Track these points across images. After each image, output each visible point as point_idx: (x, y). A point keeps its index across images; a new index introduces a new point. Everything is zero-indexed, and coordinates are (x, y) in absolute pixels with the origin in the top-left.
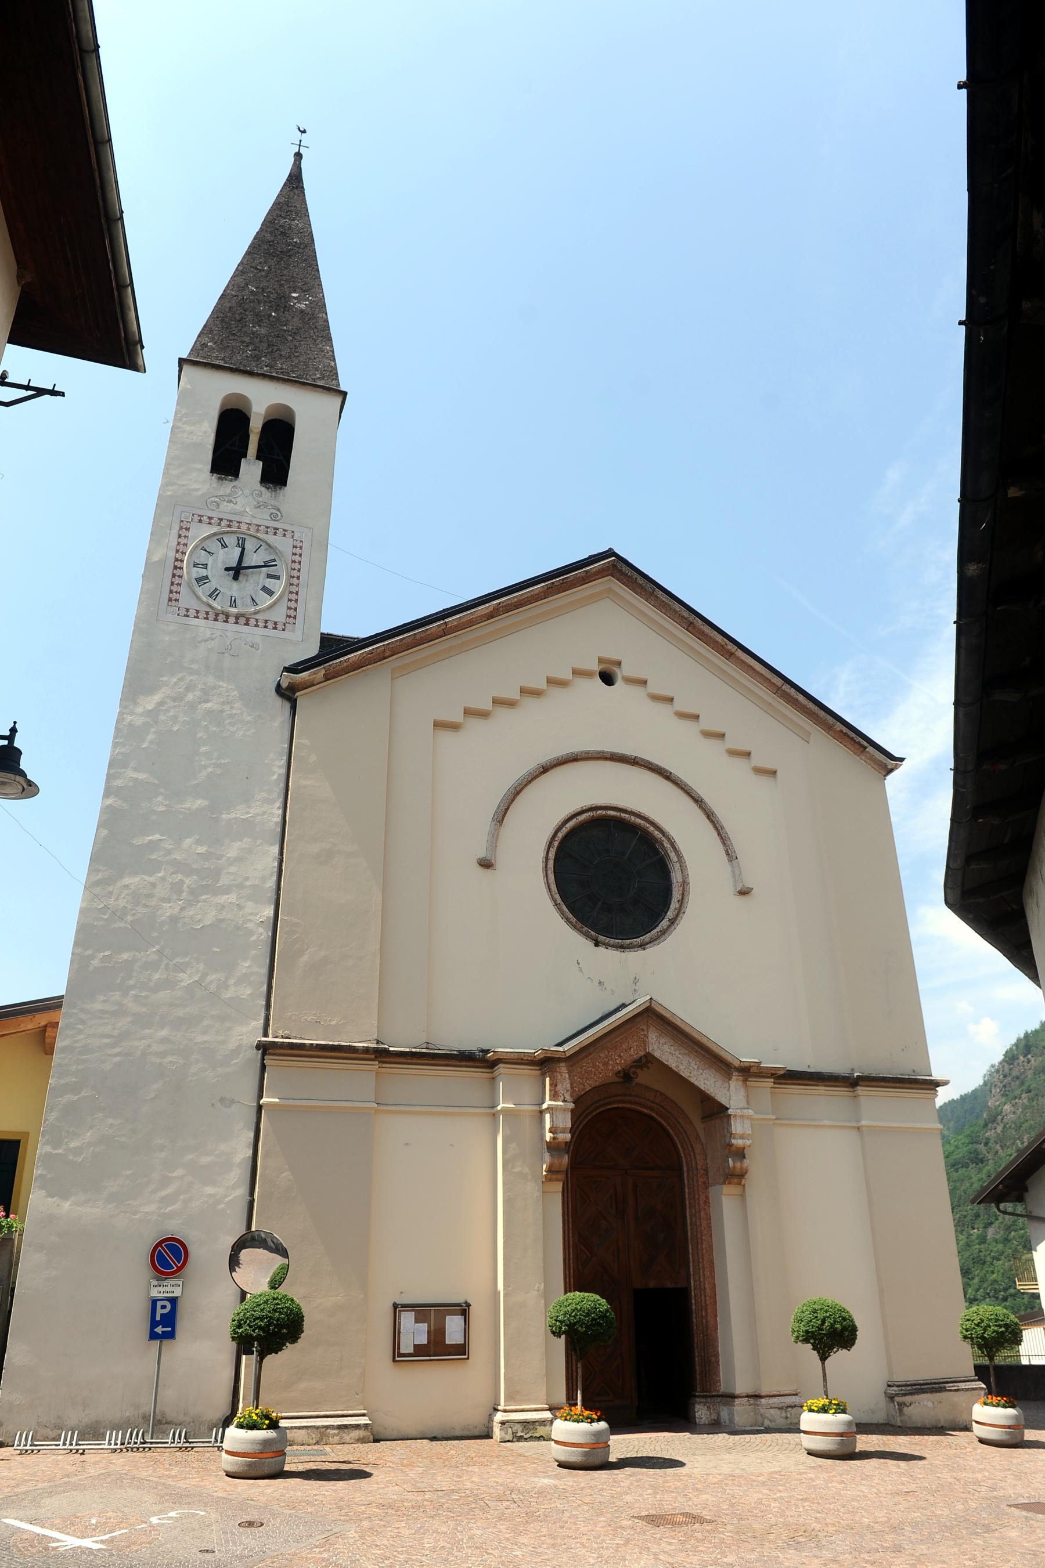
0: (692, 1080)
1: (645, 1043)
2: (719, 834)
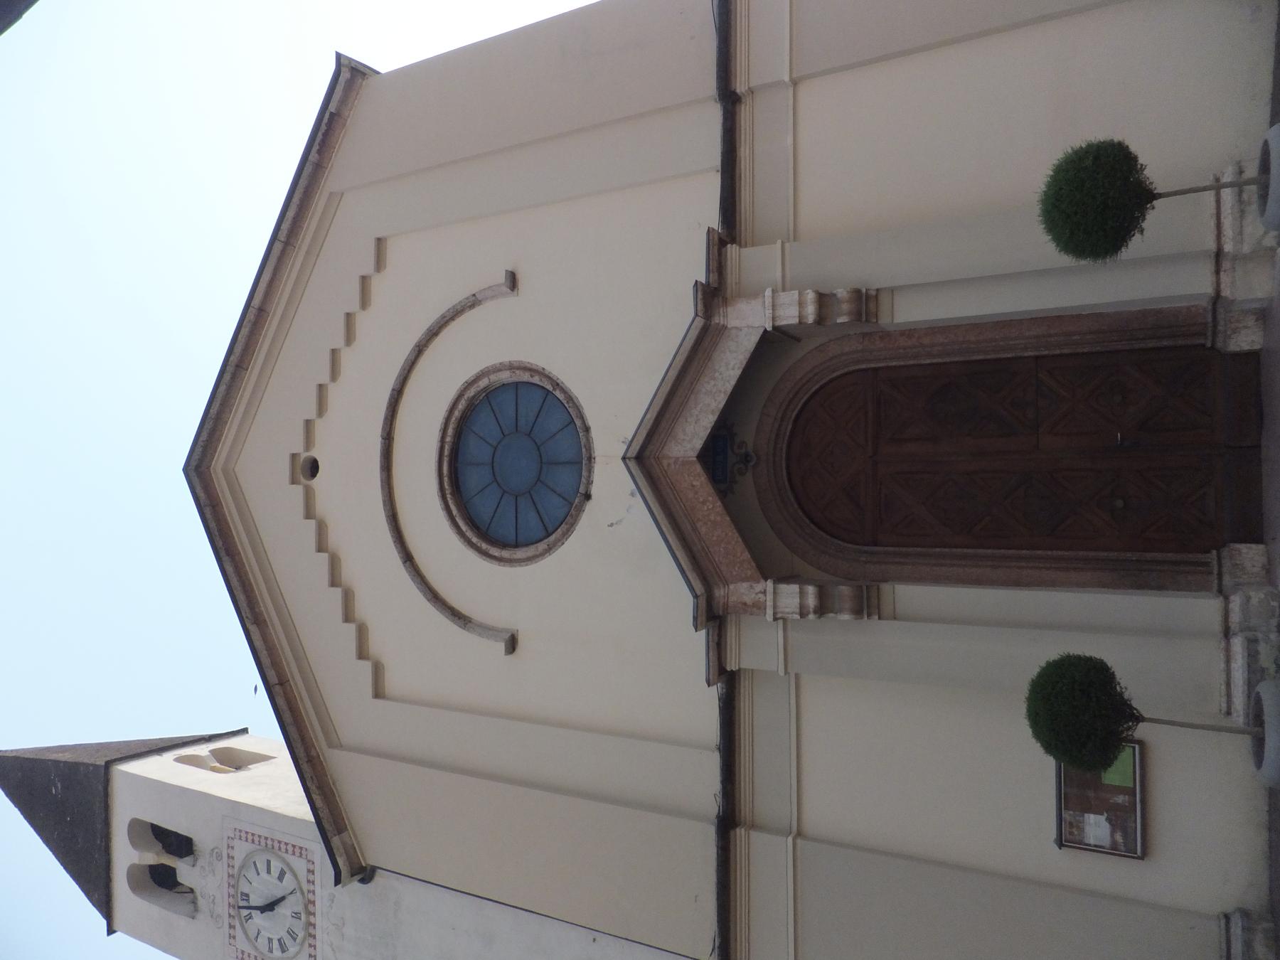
2: (452, 319)
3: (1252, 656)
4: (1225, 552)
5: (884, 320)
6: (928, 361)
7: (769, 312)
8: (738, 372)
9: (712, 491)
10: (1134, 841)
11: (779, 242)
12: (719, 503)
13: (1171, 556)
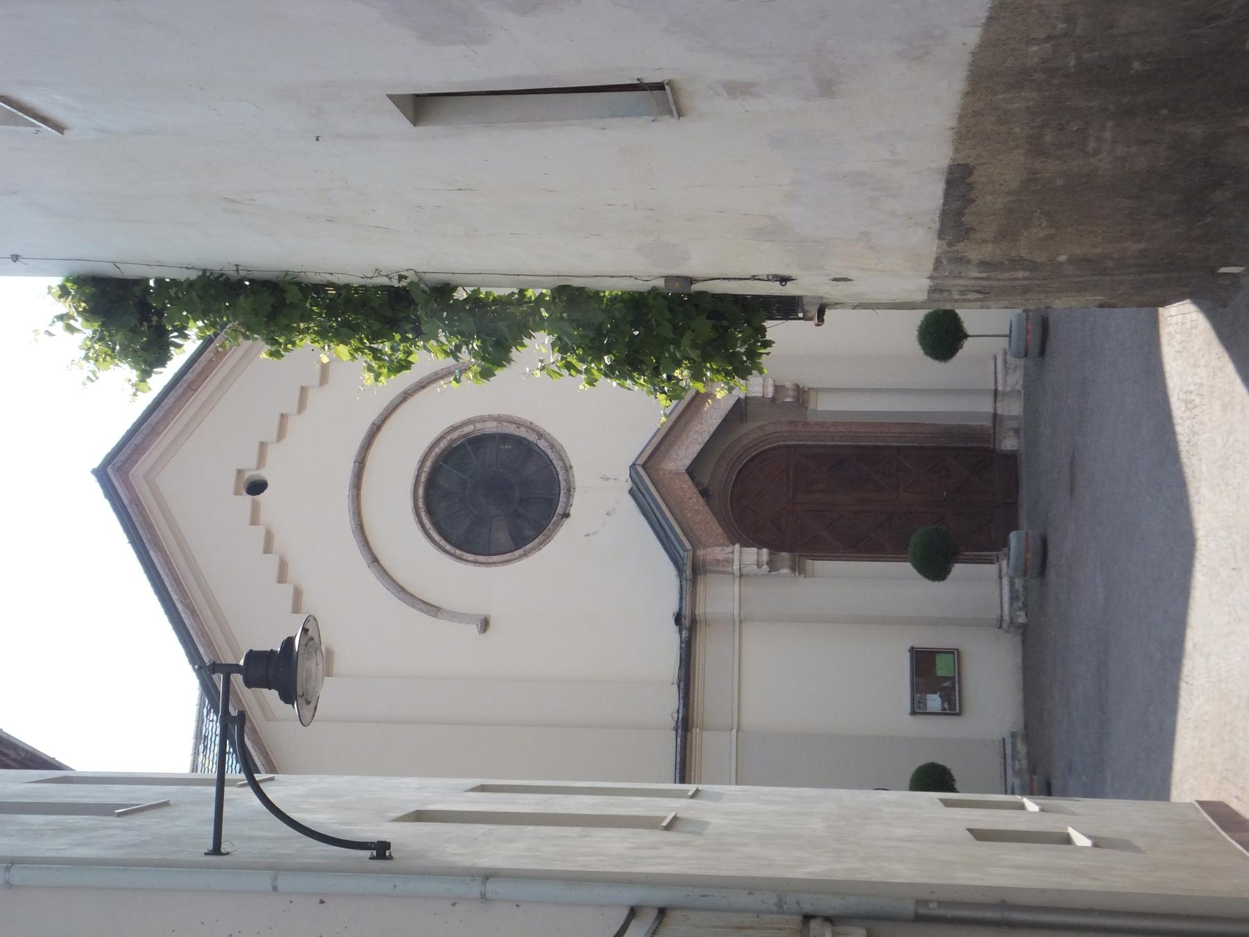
0: (712, 430)
1: (677, 474)
5: (811, 406)
8: (719, 421)
10: (953, 707)
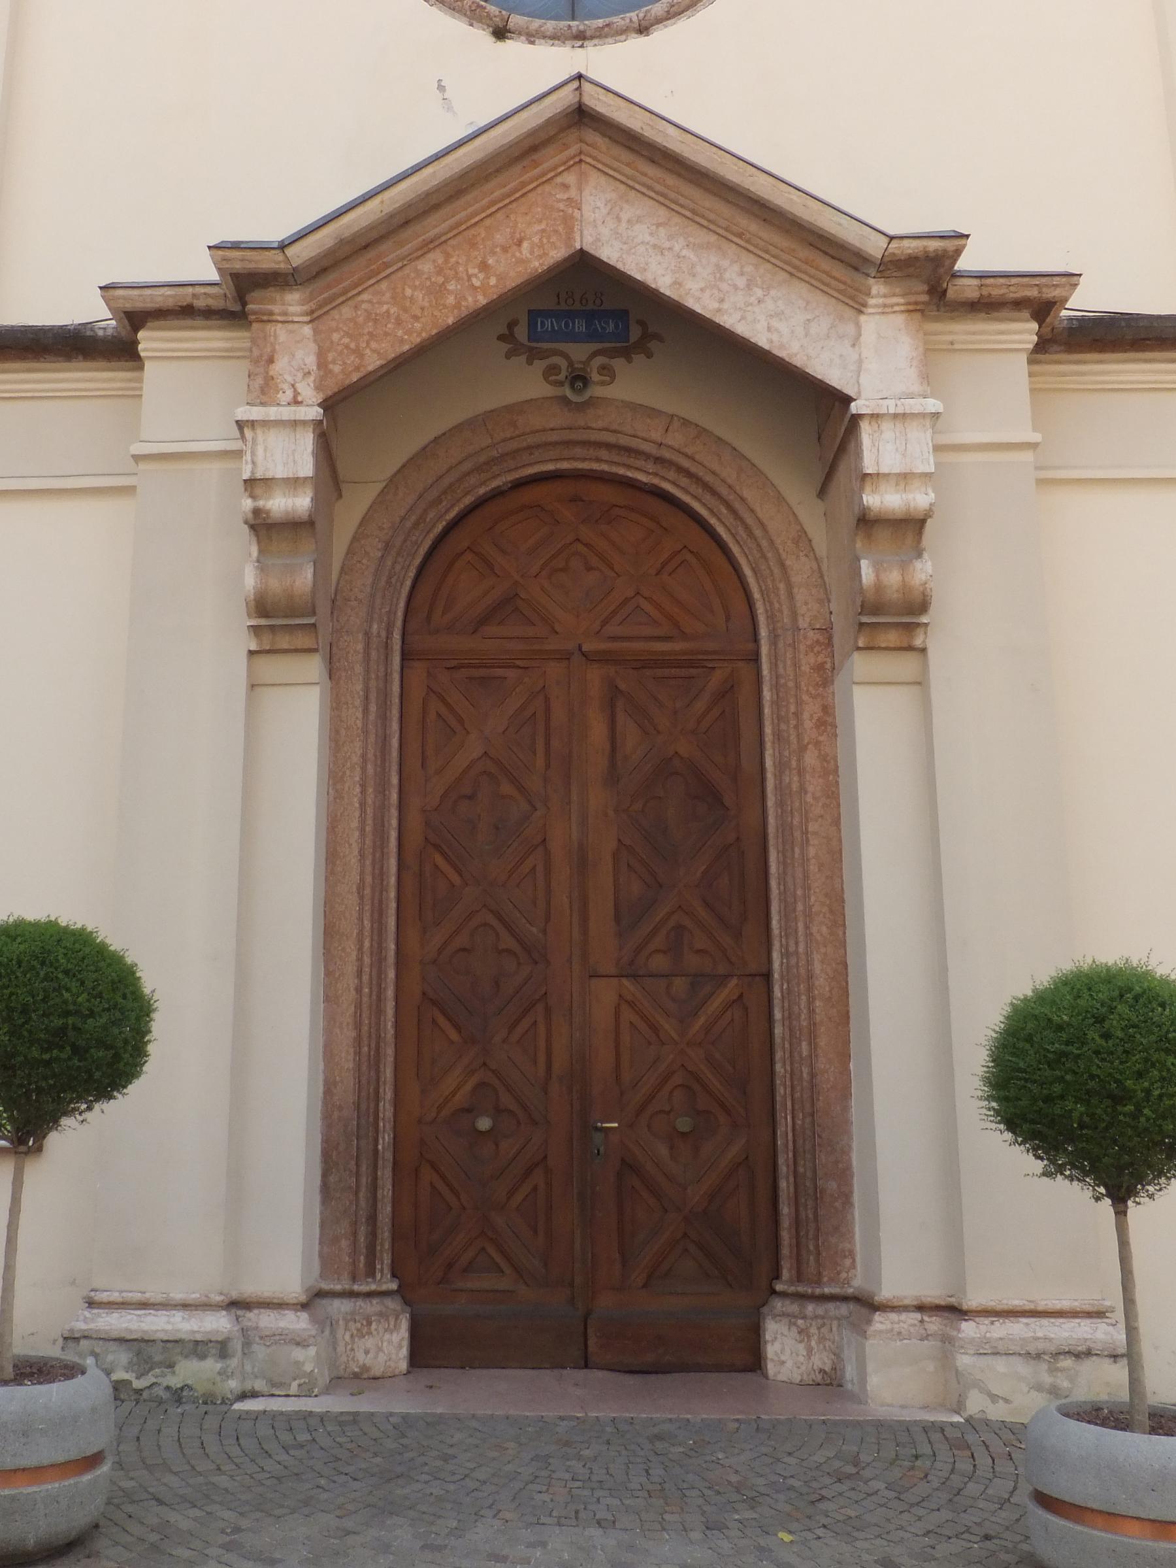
3: (197, 1348)
4: (393, 1304)
5: (861, 665)
6: (769, 763)
7: (891, 407)
9: (511, 284)
11: (1036, 437)
12: (482, 301)
13: (385, 1211)
